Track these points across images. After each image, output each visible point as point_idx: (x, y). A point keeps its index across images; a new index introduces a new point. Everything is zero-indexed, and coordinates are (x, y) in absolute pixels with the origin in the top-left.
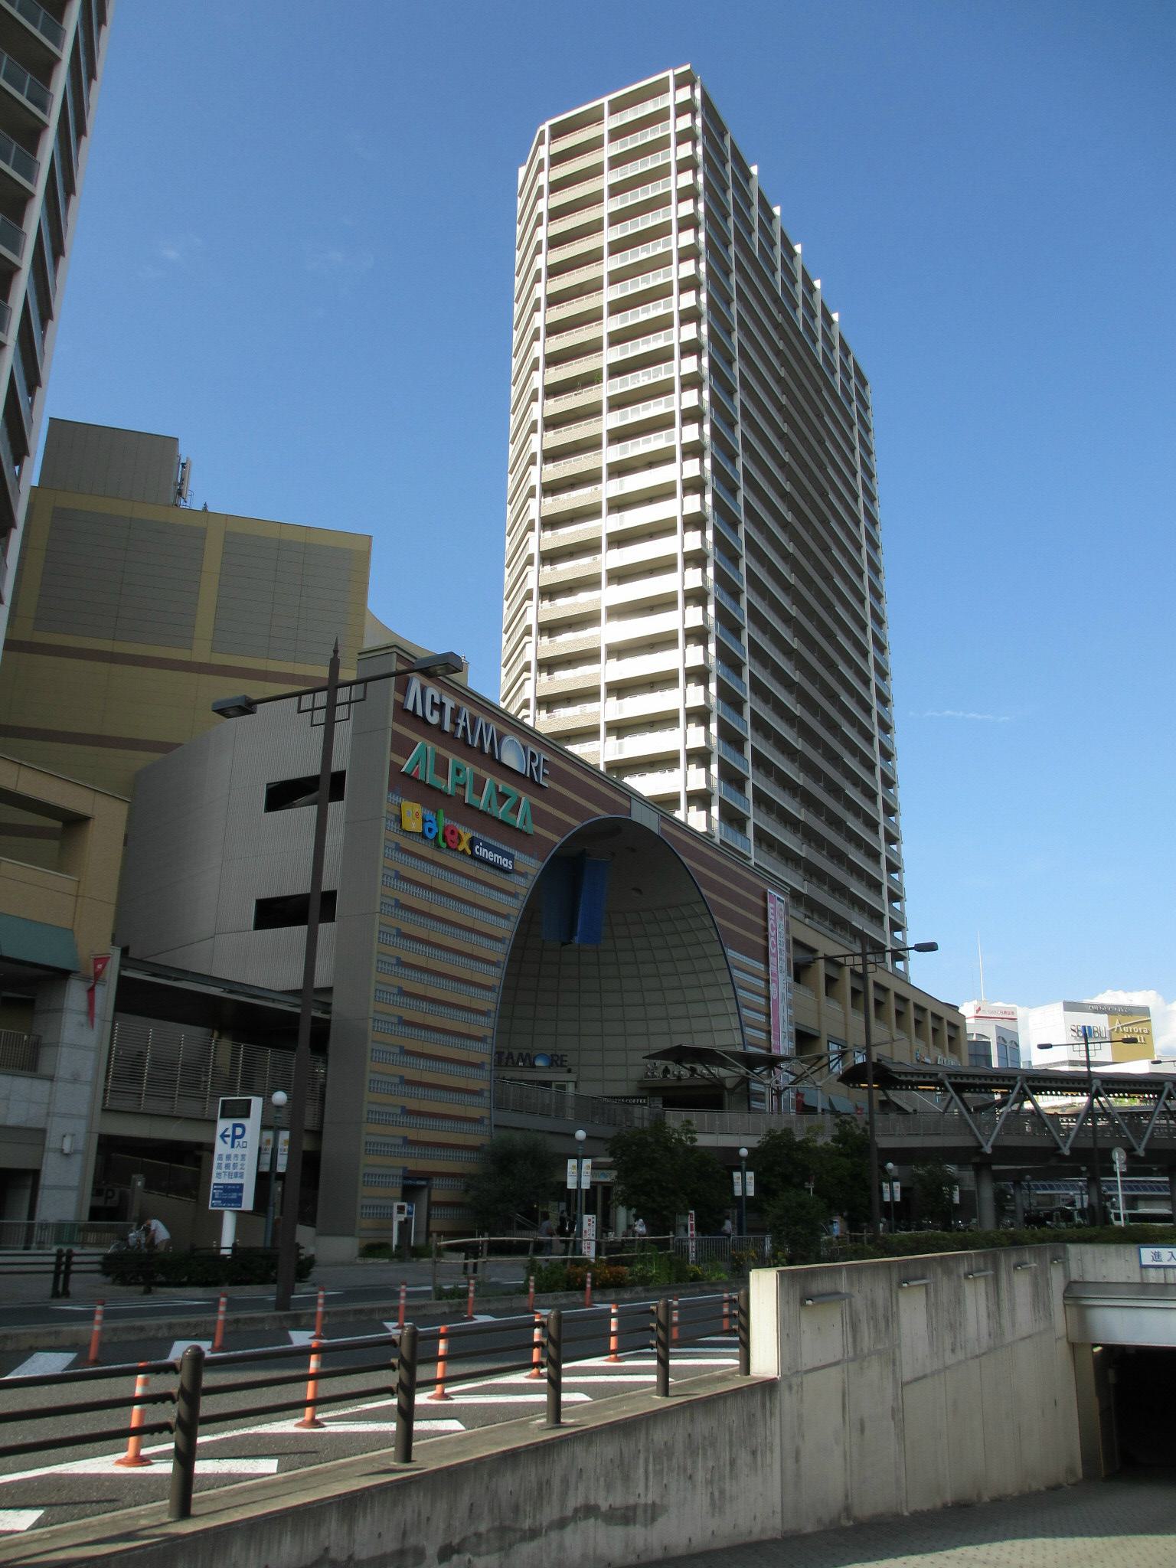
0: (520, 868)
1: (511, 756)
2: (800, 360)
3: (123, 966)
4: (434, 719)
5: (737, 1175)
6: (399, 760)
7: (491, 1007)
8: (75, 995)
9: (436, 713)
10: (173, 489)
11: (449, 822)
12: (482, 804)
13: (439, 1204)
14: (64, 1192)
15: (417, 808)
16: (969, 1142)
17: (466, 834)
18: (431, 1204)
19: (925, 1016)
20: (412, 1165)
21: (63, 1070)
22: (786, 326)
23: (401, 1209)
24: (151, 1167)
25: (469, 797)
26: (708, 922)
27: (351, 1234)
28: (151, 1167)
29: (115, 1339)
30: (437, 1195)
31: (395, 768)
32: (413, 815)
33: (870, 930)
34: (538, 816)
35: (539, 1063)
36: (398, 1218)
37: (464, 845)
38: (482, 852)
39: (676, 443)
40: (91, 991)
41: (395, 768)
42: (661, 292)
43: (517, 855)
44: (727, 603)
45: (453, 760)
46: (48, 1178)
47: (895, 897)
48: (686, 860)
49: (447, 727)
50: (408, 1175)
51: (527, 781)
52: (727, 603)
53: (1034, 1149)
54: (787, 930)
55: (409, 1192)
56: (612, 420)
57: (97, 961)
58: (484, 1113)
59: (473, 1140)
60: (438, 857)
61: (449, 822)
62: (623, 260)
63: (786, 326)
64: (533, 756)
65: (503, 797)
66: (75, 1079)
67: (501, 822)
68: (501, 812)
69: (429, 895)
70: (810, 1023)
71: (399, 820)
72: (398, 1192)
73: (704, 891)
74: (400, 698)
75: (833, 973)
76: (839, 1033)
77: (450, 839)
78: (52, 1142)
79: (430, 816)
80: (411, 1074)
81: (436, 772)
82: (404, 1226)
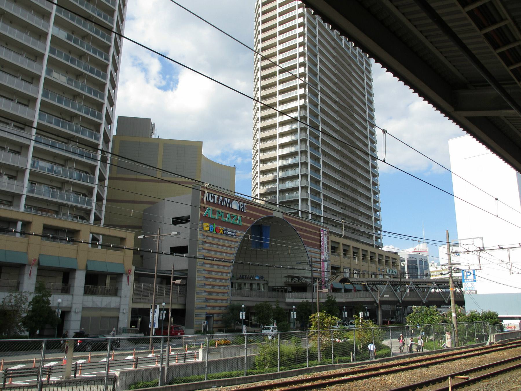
0: (238, 234)
1: (235, 206)
2: (342, 57)
3: (135, 270)
4: (212, 201)
5: (292, 313)
6: (202, 213)
7: (230, 271)
8: (125, 278)
9: (213, 199)
10: (150, 131)
11: (217, 226)
12: (227, 220)
13: (216, 320)
14: (125, 321)
15: (207, 224)
16: (372, 300)
17: (221, 228)
18: (214, 321)
19: (383, 257)
20: (208, 311)
21: (123, 295)
22: (337, 48)
23: (204, 322)
24: (140, 317)
25: (223, 219)
26: (300, 240)
27: (193, 328)
28: (140, 317)
29: (337, 318)
30: (215, 318)
31: (201, 215)
32: (207, 226)
33: (368, 231)
34: (243, 220)
35: (256, 278)
36: (203, 325)
37: (221, 231)
38: (227, 232)
39: (298, 94)
40: (128, 277)
41: (201, 215)
42: (294, 47)
43: (237, 231)
44: (314, 141)
45: (217, 209)
46: (121, 318)
47: (376, 220)
48: (291, 224)
49: (216, 202)
50: (207, 314)
51: (240, 212)
52: (314, 141)
53: (388, 301)
54: (328, 238)
55: (208, 318)
56: (280, 87)
57: (129, 270)
58: (229, 297)
59: (225, 305)
60: (214, 235)
61: (217, 226)
62: (292, 23)
63: (337, 48)
64: (242, 205)
65: (232, 217)
66: (125, 297)
67: (232, 224)
68: (232, 221)
69: (212, 245)
70: (337, 264)
71: (203, 228)
72: (205, 318)
73: (298, 232)
74: (202, 197)
75: (346, 248)
76: (348, 266)
77: (217, 231)
78: (121, 310)
79: (211, 225)
80: (207, 290)
81: (213, 214)
82: (206, 326)
